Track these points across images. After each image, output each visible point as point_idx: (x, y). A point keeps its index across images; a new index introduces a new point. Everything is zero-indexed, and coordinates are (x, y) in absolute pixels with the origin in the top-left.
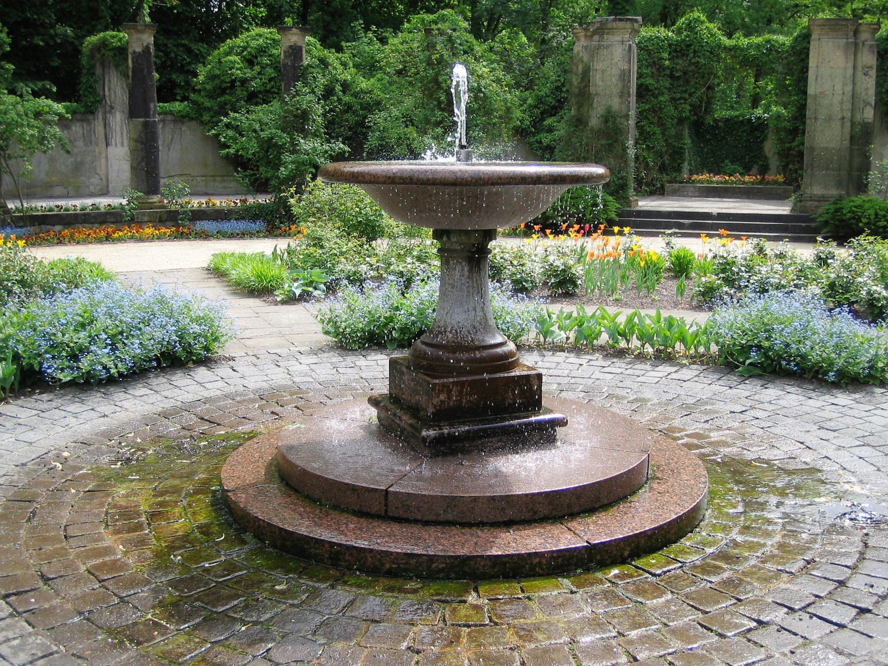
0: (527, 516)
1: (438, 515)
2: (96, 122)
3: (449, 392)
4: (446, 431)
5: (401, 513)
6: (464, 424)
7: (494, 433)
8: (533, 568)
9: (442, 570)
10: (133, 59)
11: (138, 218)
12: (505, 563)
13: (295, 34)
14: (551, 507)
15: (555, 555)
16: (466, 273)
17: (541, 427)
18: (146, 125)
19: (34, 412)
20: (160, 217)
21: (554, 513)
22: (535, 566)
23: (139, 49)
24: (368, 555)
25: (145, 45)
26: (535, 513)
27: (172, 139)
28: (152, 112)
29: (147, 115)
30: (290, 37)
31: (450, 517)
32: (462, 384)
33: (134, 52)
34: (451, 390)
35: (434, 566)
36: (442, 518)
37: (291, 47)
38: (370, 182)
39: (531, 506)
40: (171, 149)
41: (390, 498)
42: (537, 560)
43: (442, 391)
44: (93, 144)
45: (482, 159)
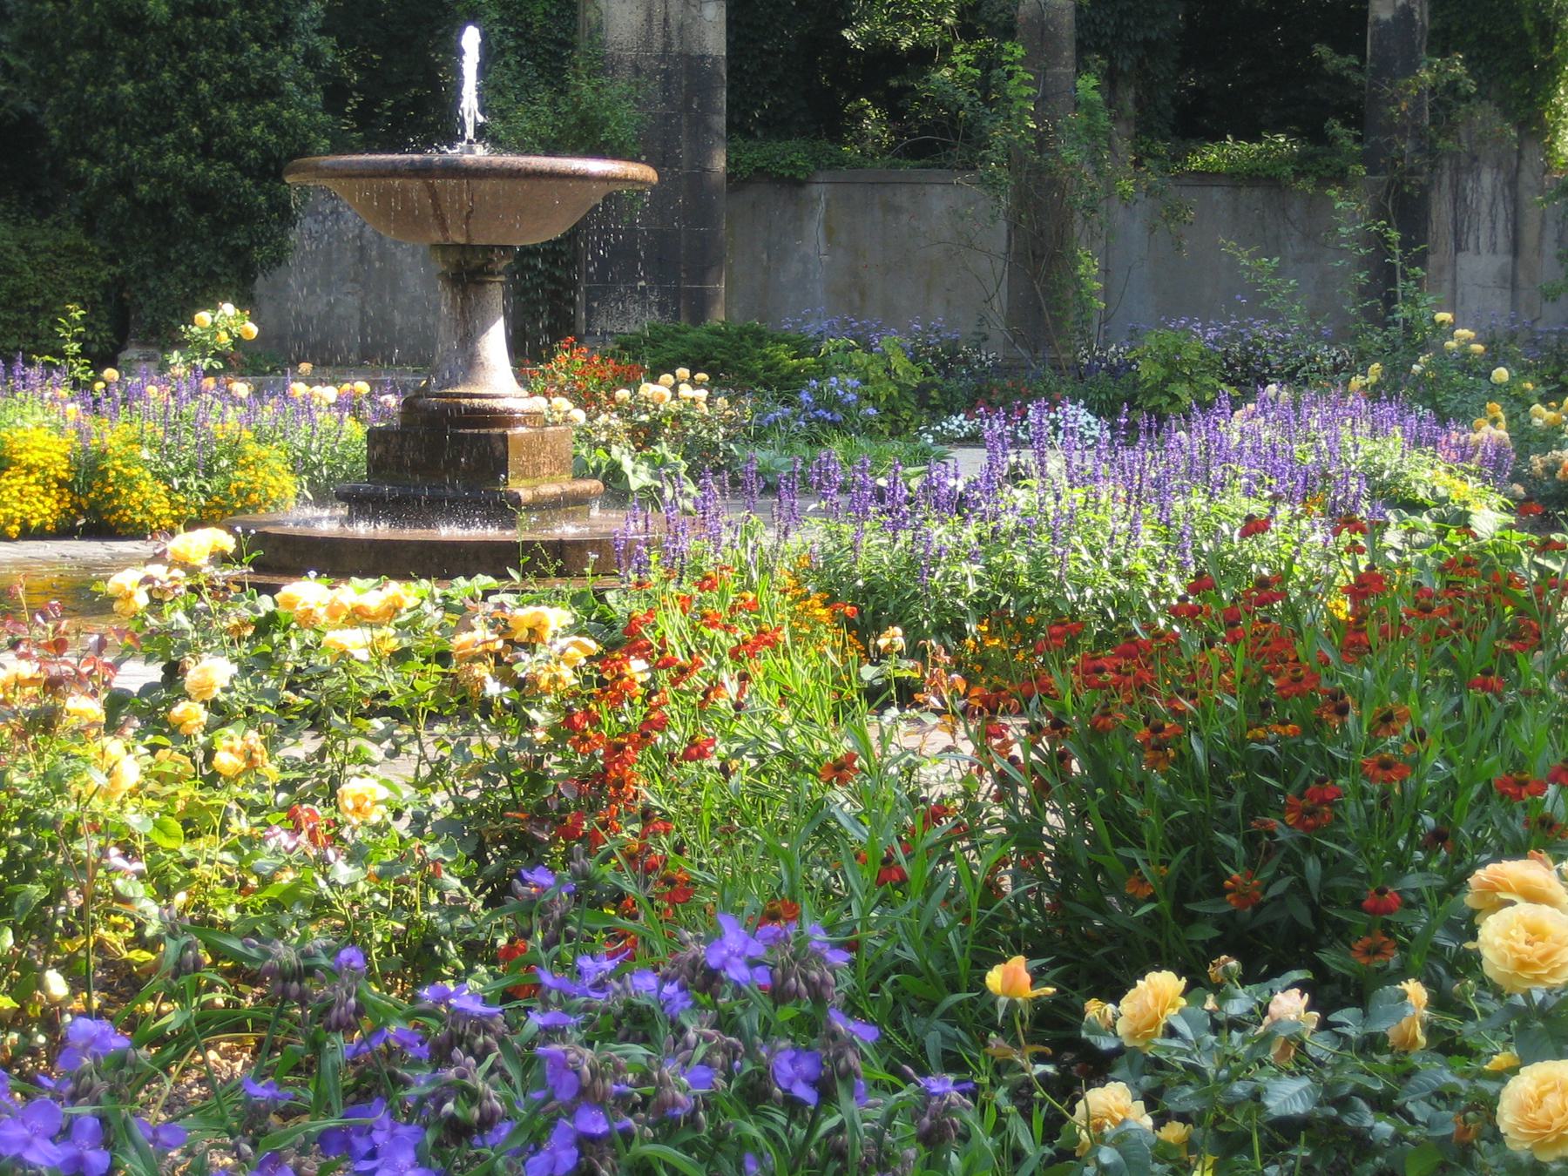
33: (1377, 22)
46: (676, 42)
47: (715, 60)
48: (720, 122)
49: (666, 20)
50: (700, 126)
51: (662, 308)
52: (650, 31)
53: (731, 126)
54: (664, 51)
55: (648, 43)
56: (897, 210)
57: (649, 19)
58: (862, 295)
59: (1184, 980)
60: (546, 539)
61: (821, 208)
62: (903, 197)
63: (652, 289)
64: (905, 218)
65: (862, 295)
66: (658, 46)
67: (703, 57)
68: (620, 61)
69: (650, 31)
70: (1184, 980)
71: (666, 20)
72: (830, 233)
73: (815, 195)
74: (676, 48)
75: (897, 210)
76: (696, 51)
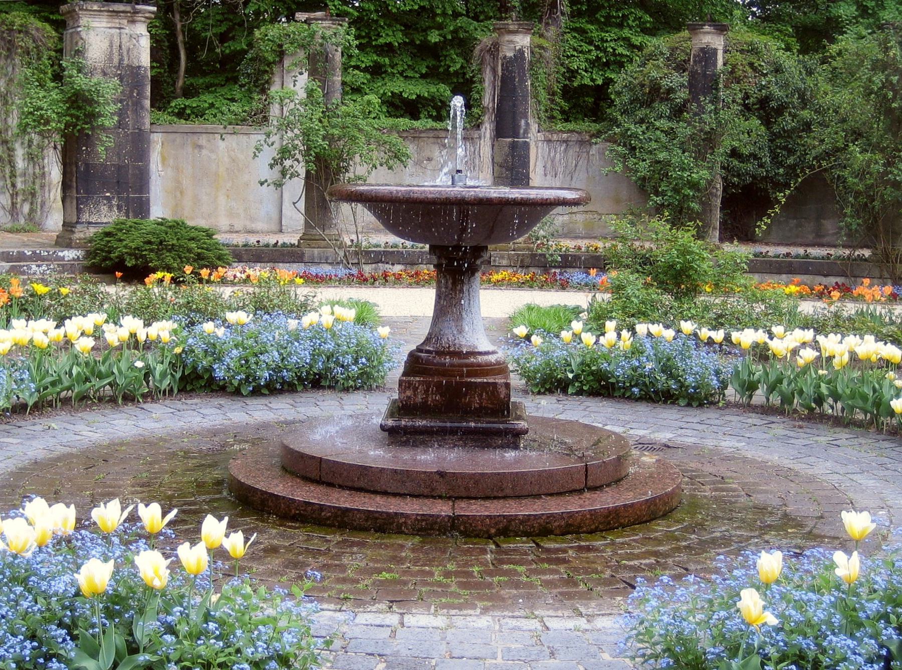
0: (426, 491)
1: (353, 481)
2: (482, 141)
3: (415, 389)
4: (403, 423)
5: (329, 479)
6: (422, 419)
7: (453, 432)
8: (399, 526)
9: (328, 519)
10: (502, 65)
11: (495, 261)
12: (377, 519)
13: (709, 33)
14: (448, 487)
15: (419, 518)
16: (450, 286)
17: (507, 432)
18: (513, 146)
19: (172, 410)
20: (522, 261)
21: (451, 493)
22: (402, 525)
23: (510, 54)
24: (282, 501)
25: (517, 48)
26: (433, 490)
27: (576, 166)
28: (522, 131)
29: (516, 134)
30: (701, 36)
31: (362, 484)
32: (428, 384)
33: (505, 57)
34: (417, 388)
35: (323, 514)
36: (356, 485)
37: (702, 49)
38: (370, 201)
39: (428, 483)
40: (574, 179)
41: (324, 465)
42: (403, 520)
43: (409, 387)
44: (477, 168)
45: (339, 179)
46: (126, 59)
47: (146, 68)
48: (147, 103)
49: (120, 46)
50: (138, 105)
51: (119, 208)
52: (111, 53)
53: (152, 106)
54: (120, 63)
55: (110, 59)
56: (200, 147)
57: (111, 46)
58: (181, 193)
59: (73, 506)
60: (401, 370)
61: (158, 147)
62: (203, 140)
63: (113, 198)
64: (204, 152)
65: (181, 193)
66: (116, 61)
67: (139, 67)
68: (95, 69)
69: (111, 53)
70: (73, 506)
71: (120, 46)
72: (164, 159)
73: (156, 139)
74: (126, 62)
75: (200, 147)
76: (136, 63)
